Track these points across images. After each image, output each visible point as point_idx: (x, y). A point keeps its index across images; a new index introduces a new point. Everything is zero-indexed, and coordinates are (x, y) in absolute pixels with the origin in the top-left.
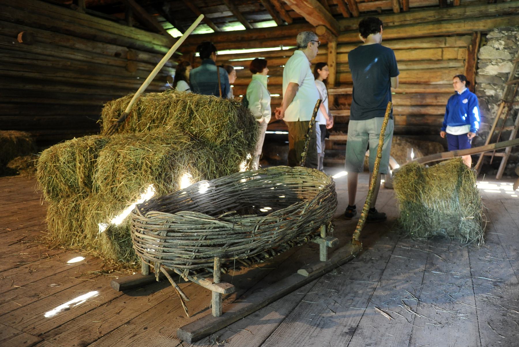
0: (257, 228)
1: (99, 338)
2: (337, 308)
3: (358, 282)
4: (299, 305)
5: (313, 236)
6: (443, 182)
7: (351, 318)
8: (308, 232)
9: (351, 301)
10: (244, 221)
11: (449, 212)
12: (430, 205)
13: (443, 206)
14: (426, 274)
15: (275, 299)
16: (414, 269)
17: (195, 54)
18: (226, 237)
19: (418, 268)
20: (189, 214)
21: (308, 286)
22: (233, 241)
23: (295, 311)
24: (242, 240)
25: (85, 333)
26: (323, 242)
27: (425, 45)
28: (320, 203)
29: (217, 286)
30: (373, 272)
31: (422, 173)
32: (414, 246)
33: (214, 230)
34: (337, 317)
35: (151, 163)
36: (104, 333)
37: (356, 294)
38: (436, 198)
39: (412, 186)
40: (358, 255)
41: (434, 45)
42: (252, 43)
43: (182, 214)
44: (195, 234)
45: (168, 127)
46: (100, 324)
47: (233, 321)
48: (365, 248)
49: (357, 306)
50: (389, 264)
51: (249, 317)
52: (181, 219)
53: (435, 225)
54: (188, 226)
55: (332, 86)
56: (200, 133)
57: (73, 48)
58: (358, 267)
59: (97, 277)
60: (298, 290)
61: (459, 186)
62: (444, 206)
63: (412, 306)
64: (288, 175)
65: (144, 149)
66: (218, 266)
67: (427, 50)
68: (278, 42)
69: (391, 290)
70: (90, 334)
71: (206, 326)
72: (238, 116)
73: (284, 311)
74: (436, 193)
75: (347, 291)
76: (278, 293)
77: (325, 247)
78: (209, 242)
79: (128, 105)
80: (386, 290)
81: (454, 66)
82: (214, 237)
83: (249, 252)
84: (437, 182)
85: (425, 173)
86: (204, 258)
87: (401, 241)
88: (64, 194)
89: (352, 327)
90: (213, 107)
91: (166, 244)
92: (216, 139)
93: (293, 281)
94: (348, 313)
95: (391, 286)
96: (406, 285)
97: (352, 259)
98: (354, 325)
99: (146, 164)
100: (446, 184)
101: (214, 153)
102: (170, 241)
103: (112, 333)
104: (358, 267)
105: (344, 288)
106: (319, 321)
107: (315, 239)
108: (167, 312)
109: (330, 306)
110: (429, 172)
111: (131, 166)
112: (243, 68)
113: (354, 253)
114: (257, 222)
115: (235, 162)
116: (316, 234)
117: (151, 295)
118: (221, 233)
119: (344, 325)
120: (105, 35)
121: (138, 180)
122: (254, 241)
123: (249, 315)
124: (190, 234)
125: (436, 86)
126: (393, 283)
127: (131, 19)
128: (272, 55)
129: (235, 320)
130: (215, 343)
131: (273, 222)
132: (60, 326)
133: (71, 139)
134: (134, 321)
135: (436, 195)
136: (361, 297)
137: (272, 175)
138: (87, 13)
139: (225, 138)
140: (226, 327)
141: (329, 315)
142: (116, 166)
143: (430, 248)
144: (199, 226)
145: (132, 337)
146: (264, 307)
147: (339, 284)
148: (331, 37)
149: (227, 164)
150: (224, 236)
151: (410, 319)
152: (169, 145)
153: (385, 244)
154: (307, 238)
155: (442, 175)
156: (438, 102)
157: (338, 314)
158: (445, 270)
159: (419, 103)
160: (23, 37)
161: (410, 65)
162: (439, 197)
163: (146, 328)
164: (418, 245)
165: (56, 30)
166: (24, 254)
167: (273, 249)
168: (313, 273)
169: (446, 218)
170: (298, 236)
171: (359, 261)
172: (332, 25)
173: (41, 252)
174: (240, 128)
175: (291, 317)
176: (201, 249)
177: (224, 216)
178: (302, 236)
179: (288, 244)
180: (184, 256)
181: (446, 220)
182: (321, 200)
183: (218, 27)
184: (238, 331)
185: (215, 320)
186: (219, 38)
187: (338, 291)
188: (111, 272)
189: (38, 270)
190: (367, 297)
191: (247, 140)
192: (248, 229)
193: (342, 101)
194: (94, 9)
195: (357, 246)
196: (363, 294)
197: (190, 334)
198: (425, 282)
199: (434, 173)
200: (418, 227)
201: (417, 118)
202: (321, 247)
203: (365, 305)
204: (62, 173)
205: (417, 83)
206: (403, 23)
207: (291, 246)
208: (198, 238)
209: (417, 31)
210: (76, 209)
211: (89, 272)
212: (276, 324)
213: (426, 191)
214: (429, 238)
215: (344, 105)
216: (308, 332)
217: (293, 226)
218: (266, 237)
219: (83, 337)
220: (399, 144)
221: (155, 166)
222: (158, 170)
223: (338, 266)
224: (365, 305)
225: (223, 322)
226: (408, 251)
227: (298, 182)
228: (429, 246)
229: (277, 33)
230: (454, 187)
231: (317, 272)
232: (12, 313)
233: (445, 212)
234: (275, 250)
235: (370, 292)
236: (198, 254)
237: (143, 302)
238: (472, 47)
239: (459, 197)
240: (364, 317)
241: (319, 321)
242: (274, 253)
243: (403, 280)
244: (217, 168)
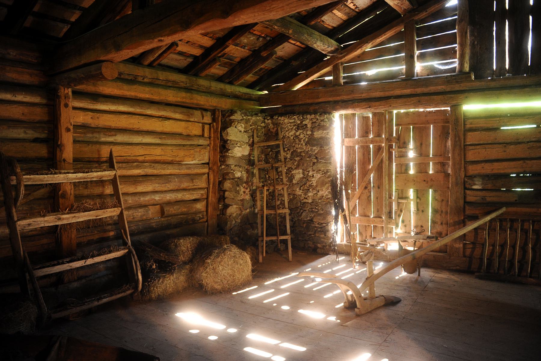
27: (178, 116)
67: (179, 123)
112: (502, 128)
161: (164, 138)
209: (171, 96)
238: (216, 124)
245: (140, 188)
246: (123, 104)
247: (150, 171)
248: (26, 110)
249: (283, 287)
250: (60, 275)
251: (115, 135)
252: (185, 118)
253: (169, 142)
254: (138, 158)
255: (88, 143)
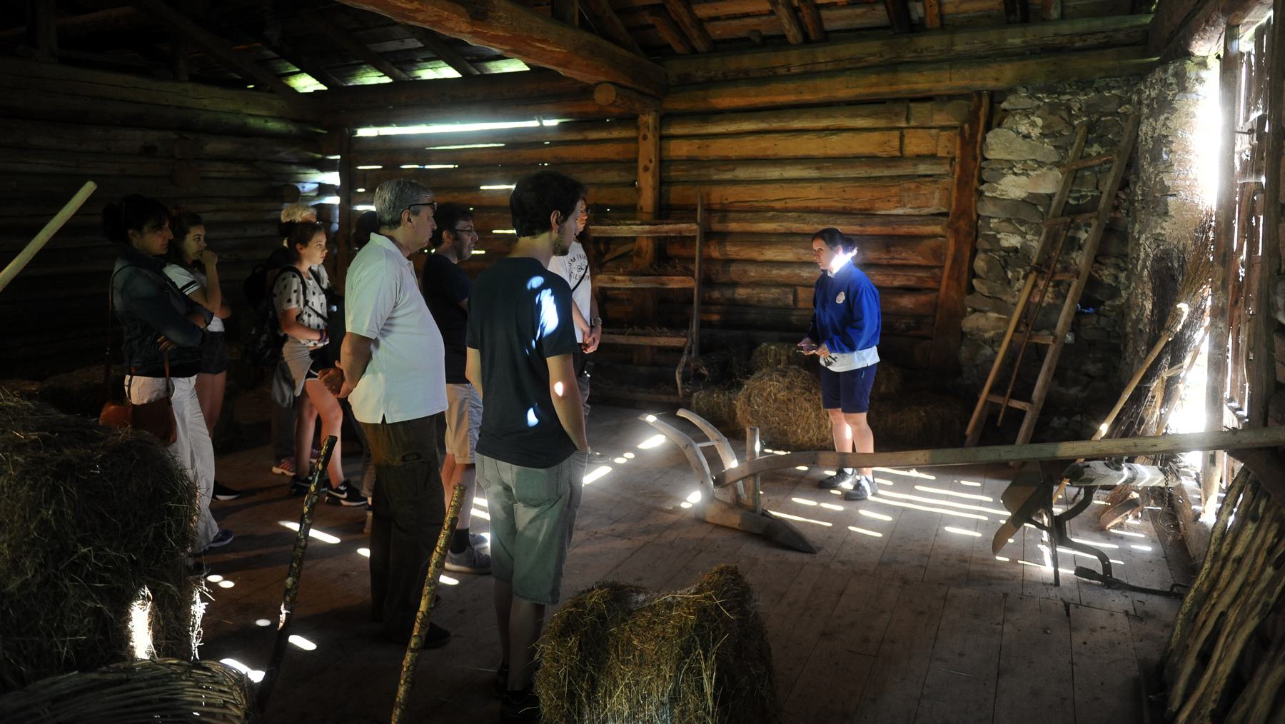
67: (865, 135)
209: (843, 89)
245: (770, 254)
246: (749, 119)
247: (796, 227)
248: (618, 148)
249: (917, 487)
250: (628, 349)
251: (733, 170)
252: (882, 123)
253: (840, 173)
254: (772, 204)
255: (696, 183)
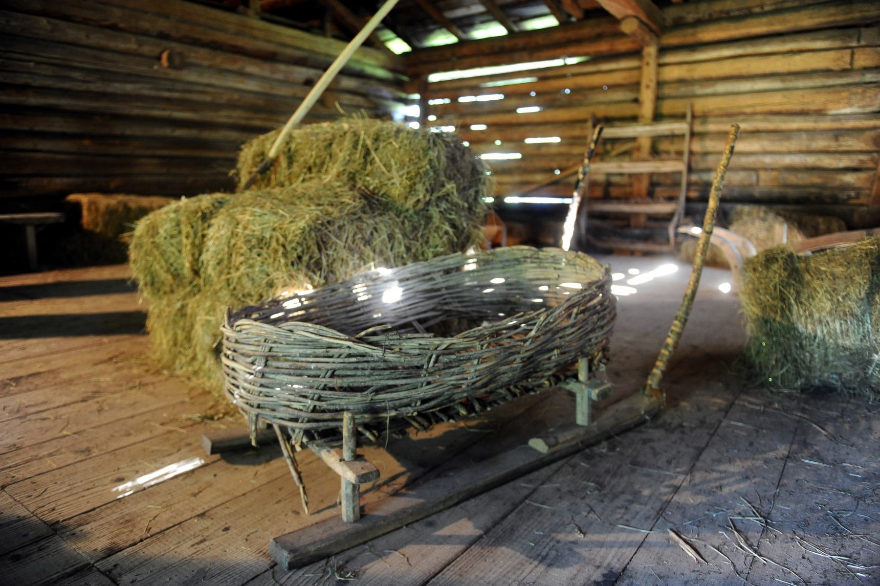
0: (433, 360)
1: (141, 541)
2: (591, 524)
3: (646, 470)
4: (517, 510)
5: (562, 377)
6: (841, 284)
7: (614, 550)
8: (549, 369)
9: (623, 511)
10: (407, 345)
11: (847, 343)
12: (809, 327)
13: (836, 333)
14: (790, 464)
15: (472, 495)
16: (765, 452)
17: (427, 78)
18: (372, 375)
19: (775, 449)
20: (303, 328)
21: (545, 472)
22: (384, 383)
23: (505, 523)
24: (404, 381)
25: (124, 528)
26: (582, 390)
28: (573, 316)
29: (345, 468)
30: (679, 452)
31: (798, 265)
32: (771, 403)
33: (347, 360)
34: (585, 545)
35: (285, 237)
36: (154, 530)
37: (636, 496)
38: (824, 314)
39: (775, 289)
40: (655, 415)
41: (837, 44)
42: (516, 55)
43: (290, 328)
44: (313, 366)
45: (327, 179)
46: (157, 512)
47: (381, 533)
48: (673, 401)
49: (633, 523)
50: (716, 438)
51: (416, 525)
52: (288, 337)
53: (819, 366)
54: (301, 351)
55: (649, 121)
56: (381, 186)
57: (241, 74)
58: (651, 440)
59: (192, 425)
60: (522, 479)
61: (873, 294)
62: (838, 331)
63: (750, 534)
64: (532, 262)
65: (276, 213)
66: (349, 430)
67: (823, 54)
68: (558, 51)
69: (710, 493)
70: (132, 531)
71: (322, 541)
72: (447, 157)
73: (485, 519)
74: (823, 304)
75: (620, 489)
76: (480, 483)
77: (586, 399)
78: (337, 382)
79: (274, 145)
80: (699, 492)
81: (874, 80)
82: (349, 373)
83: (419, 403)
84: (826, 284)
85: (803, 265)
86: (330, 411)
87: (747, 393)
88: (167, 289)
89: (611, 572)
90: (402, 142)
91: (263, 381)
92: (406, 198)
93: (513, 460)
94: (611, 537)
95: (712, 485)
96: (743, 486)
97: (642, 423)
98: (618, 566)
99: (277, 240)
100: (847, 287)
101: (403, 223)
102: (272, 376)
103: (167, 532)
104: (651, 440)
105: (614, 481)
106: (547, 549)
107: (568, 384)
108: (275, 501)
109: (577, 519)
110: (812, 265)
111: (254, 242)
113: (647, 412)
114: (432, 348)
115: (441, 238)
116: (569, 373)
117: (263, 465)
118: (360, 366)
119: (597, 563)
120: (289, 52)
121: (265, 267)
122: (429, 383)
123: (417, 521)
124: (304, 365)
125: (837, 117)
126: (716, 479)
127: (329, 26)
128: (550, 73)
129: (385, 531)
130: (333, 574)
131: (466, 349)
132: (94, 509)
133: (178, 197)
134: (212, 512)
135: (823, 309)
136: (646, 504)
137: (501, 262)
138: (263, 19)
139: (421, 196)
140: (365, 543)
141: (571, 538)
142: (233, 242)
143: (803, 410)
144: (320, 351)
145: (197, 544)
146: (449, 507)
147: (607, 472)
148: (647, 38)
149: (427, 242)
150: (367, 372)
151: (740, 565)
152: (321, 208)
153: (714, 396)
154: (549, 380)
155: (839, 270)
156: (840, 146)
157: (590, 537)
158: (830, 458)
159: (804, 148)
160: (170, 59)
161: (790, 81)
162: (830, 313)
163: (227, 529)
164: (779, 402)
165: (216, 47)
166: (105, 380)
167: (478, 400)
168: (558, 447)
169: (841, 354)
170: (527, 376)
171: (657, 427)
172: (649, 15)
173: (133, 377)
174: (450, 178)
175: (493, 535)
176: (324, 394)
177: (367, 335)
178: (537, 377)
179: (509, 390)
180: (295, 405)
181: (840, 358)
182: (575, 310)
183: (464, 32)
184: (384, 554)
185: (343, 528)
186: (465, 50)
187: (601, 486)
188: (219, 419)
189: (112, 407)
190: (658, 505)
191: (467, 201)
192: (416, 362)
193: (664, 146)
194: (275, 14)
195: (654, 399)
196: (650, 497)
197: (285, 553)
198: (785, 481)
199: (823, 266)
200: (782, 368)
201: (800, 175)
202: (578, 399)
203: (650, 523)
204: (163, 254)
205: (803, 113)
206: (779, 6)
207: (514, 395)
208: (318, 372)
210: (182, 312)
211: (184, 416)
212: (459, 548)
213: (803, 300)
214: (803, 390)
215: (667, 152)
216: (519, 572)
217: (511, 358)
218: (453, 378)
219: (117, 535)
220: (764, 220)
221: (291, 242)
222: (296, 250)
223: (612, 436)
224: (650, 523)
225: (358, 533)
226: (758, 412)
227: (550, 276)
228: (803, 405)
229: (559, 36)
230: (863, 294)
231: (566, 445)
232: (36, 479)
233: (840, 342)
234: (480, 400)
235: (665, 494)
236: (318, 403)
237: (247, 476)
239: (871, 314)
240: (641, 549)
241: (547, 549)
242: (477, 407)
243: (739, 473)
244: (408, 249)
